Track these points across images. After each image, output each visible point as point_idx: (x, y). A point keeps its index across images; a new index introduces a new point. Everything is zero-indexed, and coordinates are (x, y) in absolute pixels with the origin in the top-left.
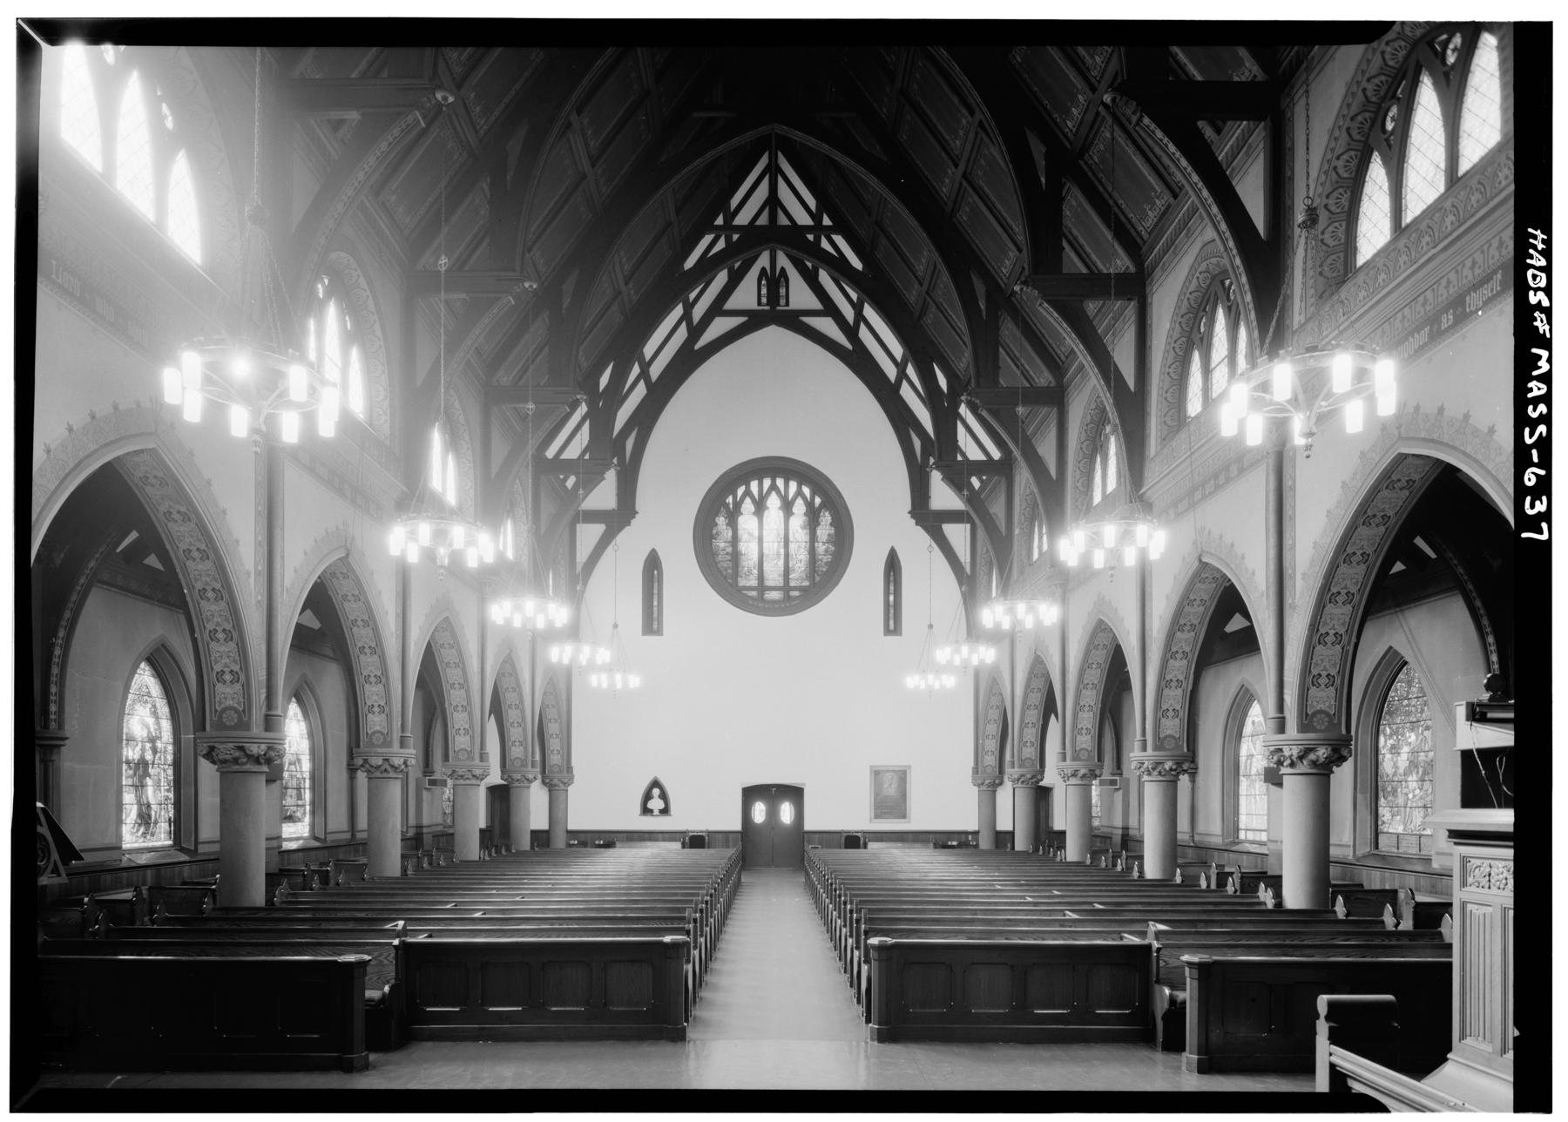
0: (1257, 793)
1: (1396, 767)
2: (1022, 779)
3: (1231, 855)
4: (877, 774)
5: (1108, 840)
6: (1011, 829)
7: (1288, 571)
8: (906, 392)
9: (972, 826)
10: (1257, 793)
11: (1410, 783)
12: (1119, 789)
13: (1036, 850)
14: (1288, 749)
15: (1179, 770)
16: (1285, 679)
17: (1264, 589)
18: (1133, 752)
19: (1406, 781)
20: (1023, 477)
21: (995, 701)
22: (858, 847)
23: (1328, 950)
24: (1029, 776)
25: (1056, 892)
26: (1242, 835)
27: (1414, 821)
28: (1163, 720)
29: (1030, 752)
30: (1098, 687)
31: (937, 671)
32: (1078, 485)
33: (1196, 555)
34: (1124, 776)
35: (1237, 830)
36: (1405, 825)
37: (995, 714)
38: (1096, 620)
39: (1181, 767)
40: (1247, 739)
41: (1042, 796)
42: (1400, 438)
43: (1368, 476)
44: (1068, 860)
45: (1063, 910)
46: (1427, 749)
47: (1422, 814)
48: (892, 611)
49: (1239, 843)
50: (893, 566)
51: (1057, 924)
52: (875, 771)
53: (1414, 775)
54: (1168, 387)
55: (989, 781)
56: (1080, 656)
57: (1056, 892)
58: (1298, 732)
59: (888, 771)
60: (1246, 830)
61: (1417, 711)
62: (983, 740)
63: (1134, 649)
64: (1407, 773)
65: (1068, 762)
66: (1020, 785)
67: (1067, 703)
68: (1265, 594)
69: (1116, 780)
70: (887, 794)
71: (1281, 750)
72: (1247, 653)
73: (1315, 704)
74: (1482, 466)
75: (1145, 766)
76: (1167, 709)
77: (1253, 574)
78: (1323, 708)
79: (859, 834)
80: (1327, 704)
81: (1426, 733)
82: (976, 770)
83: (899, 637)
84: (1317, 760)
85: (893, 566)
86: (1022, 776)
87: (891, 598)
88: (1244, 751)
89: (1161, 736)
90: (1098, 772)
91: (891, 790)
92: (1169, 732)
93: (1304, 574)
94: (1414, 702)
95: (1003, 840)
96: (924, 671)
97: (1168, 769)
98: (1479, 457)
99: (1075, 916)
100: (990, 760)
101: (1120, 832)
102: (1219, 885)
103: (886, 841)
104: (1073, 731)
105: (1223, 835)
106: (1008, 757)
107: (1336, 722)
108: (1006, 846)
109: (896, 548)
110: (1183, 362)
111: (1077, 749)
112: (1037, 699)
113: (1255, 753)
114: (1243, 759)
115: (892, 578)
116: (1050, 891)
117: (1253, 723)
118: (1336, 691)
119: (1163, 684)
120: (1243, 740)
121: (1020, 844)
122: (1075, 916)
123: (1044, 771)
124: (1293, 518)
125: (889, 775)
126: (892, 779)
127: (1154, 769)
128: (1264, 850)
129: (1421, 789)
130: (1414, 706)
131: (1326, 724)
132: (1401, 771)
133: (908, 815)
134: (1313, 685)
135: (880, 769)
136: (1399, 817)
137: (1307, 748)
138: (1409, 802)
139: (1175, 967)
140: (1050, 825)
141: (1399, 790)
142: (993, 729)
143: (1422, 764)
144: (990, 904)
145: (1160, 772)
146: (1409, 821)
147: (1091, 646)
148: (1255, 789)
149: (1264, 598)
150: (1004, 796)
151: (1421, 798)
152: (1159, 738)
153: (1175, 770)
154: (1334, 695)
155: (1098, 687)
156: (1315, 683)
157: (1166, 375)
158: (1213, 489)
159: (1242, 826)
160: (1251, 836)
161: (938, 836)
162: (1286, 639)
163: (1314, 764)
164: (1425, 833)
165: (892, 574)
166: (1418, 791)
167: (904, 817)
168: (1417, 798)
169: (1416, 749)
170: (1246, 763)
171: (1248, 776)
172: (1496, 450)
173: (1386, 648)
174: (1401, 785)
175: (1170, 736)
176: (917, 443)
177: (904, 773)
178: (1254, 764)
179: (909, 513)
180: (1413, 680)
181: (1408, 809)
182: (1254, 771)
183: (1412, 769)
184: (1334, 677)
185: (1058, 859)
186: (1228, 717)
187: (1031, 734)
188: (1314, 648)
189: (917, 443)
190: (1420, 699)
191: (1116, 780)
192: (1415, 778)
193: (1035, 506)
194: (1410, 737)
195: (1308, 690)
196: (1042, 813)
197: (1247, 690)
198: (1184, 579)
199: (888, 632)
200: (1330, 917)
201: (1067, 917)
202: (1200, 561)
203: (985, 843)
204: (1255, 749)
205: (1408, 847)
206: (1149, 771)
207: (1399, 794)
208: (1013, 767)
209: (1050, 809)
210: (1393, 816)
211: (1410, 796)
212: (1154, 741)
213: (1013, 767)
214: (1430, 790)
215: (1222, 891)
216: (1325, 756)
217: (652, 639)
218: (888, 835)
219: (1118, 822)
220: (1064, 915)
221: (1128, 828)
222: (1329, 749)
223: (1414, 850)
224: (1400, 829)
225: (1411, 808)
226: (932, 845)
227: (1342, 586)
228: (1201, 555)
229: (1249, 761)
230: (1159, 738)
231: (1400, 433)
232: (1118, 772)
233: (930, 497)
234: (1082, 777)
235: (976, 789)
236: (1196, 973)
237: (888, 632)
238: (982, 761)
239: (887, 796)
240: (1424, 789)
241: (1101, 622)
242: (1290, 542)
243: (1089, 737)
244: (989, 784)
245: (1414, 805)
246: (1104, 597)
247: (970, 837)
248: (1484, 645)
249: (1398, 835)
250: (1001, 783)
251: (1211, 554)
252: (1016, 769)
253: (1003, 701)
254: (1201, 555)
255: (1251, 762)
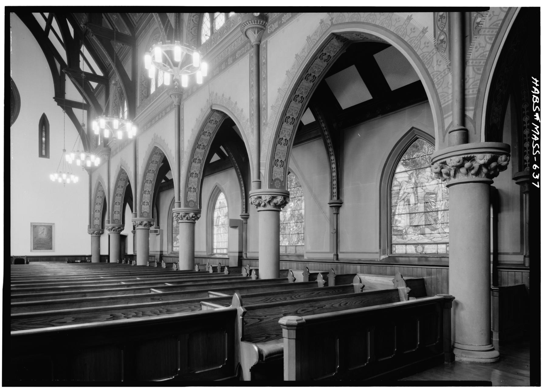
0: (222, 233)
1: (285, 217)
2: (113, 229)
3: (211, 260)
4: (34, 227)
5: (153, 258)
6: (107, 253)
7: (263, 106)
8: (51, 36)
9: (88, 253)
10: (222, 233)
11: (291, 224)
12: (159, 234)
13: (120, 261)
14: (264, 197)
15: (196, 217)
16: (261, 162)
17: (249, 117)
18: (174, 208)
19: (289, 223)
20: (116, 81)
21: (100, 194)
22: (24, 263)
23: (331, 301)
24: (117, 228)
25: (138, 279)
26: (215, 251)
27: (293, 241)
28: (189, 193)
29: (118, 216)
30: (153, 182)
31: (68, 173)
32: (143, 93)
33: (209, 106)
34: (161, 228)
35: (213, 249)
36: (289, 242)
37: (100, 201)
38: (153, 147)
39: (197, 216)
40: (217, 210)
41: (123, 239)
42: (333, 25)
43: (312, 49)
44: (138, 265)
45: (149, 288)
46: (299, 209)
47: (297, 237)
48: (44, 146)
49: (214, 255)
50: (44, 123)
51: (149, 298)
52: (34, 226)
53: (293, 221)
54: (192, 27)
55: (97, 232)
56: (144, 166)
57: (138, 279)
58: (269, 188)
59: (41, 226)
60: (217, 249)
61: (294, 193)
62: (94, 213)
63: (174, 159)
64: (290, 219)
65: (138, 217)
66: (112, 232)
67: (137, 194)
68: (249, 120)
69: (157, 230)
70: (41, 237)
71: (260, 198)
72: (218, 172)
73: (275, 175)
74: (386, 30)
75: (180, 215)
76: (191, 188)
77: (242, 111)
78: (279, 178)
79: (24, 258)
80: (280, 175)
81: (298, 202)
82: (90, 226)
83: (48, 159)
84: (277, 203)
85: (44, 123)
86: (113, 227)
87: (44, 139)
88: (216, 214)
89: (188, 200)
90: (152, 223)
91: (43, 234)
92: (191, 199)
93: (272, 107)
94: (293, 189)
95: (103, 259)
96: (61, 172)
97: (191, 216)
98: (385, 26)
99: (159, 292)
100: (97, 222)
101: (159, 253)
102: (221, 271)
103: (40, 261)
104: (140, 203)
105: (207, 252)
106: (106, 218)
107: (283, 185)
108: (105, 261)
109: (46, 114)
110: (198, 27)
111: (142, 212)
112: (121, 191)
113: (221, 216)
114: (215, 219)
115: (44, 129)
116: (135, 278)
117: (220, 203)
118: (284, 169)
119: (189, 174)
120: (215, 210)
121: (112, 260)
122: (159, 292)
123: (124, 226)
124: (266, 79)
125: (42, 228)
126: (44, 230)
127: (184, 216)
128: (226, 257)
129: (296, 226)
130: (293, 191)
131: (280, 186)
132: (287, 219)
133: (53, 248)
134: (275, 165)
135: (37, 224)
136: (286, 239)
137: (272, 197)
138: (291, 232)
139: (251, 325)
140: (126, 252)
141: (286, 227)
142: (99, 208)
143: (297, 215)
144: (96, 287)
145: (187, 218)
146: (291, 241)
147: (150, 161)
148: (221, 231)
149: (249, 123)
150: (104, 239)
151: (296, 230)
152: (187, 201)
153: (194, 217)
154: (283, 172)
155: (153, 182)
156: (276, 164)
157: (191, 21)
158: (218, 73)
159: (215, 247)
160: (219, 251)
161: (70, 258)
162: (261, 142)
163: (276, 205)
164: (298, 245)
165: (44, 127)
166: (295, 227)
167: (51, 249)
168: (295, 230)
169: (294, 209)
170: (217, 220)
171: (217, 226)
172: (396, 20)
173: (65, 321)
174: (287, 225)
175: (192, 201)
176: (58, 66)
177: (51, 227)
178: (220, 220)
179: (54, 98)
180: (292, 181)
181: (290, 235)
182: (220, 223)
183: (292, 218)
184: (283, 162)
185: (133, 264)
186: (209, 200)
187: (118, 208)
188: (276, 145)
189: (58, 66)
190: (296, 188)
191: (157, 230)
192: (293, 221)
193: (121, 94)
194: (291, 204)
195: (273, 167)
196: (122, 247)
197: (218, 188)
198: (202, 120)
199: (41, 155)
200: (285, 282)
201: (152, 293)
202: (211, 108)
203: (94, 260)
204: (221, 214)
205: (291, 251)
206: (182, 217)
207: (286, 229)
208: (109, 223)
209: (126, 245)
210: (283, 238)
211: (291, 229)
212: (185, 203)
213: (109, 223)
214: (300, 226)
215: (222, 274)
216: (281, 201)
217: (43, 219)
218: (42, 258)
219: (159, 249)
220: (150, 291)
221: (162, 252)
222: (283, 197)
223: (293, 252)
224: (287, 244)
225: (292, 234)
226: (67, 262)
227: (291, 114)
228: (212, 106)
229: (218, 219)
230: (187, 201)
231: (332, 23)
232: (158, 227)
233: (65, 80)
234: (144, 225)
235: (90, 235)
236: (293, 333)
237: (41, 155)
238: (93, 222)
239: (40, 238)
240: (298, 226)
241: (156, 148)
242: (264, 91)
243: (148, 206)
244: (98, 233)
245: (293, 233)
246: (157, 135)
247: (87, 258)
248: (330, 160)
249: (286, 246)
250: (103, 233)
251: (217, 104)
252: (110, 224)
253: (104, 193)
254: (212, 106)
255: (219, 220)
